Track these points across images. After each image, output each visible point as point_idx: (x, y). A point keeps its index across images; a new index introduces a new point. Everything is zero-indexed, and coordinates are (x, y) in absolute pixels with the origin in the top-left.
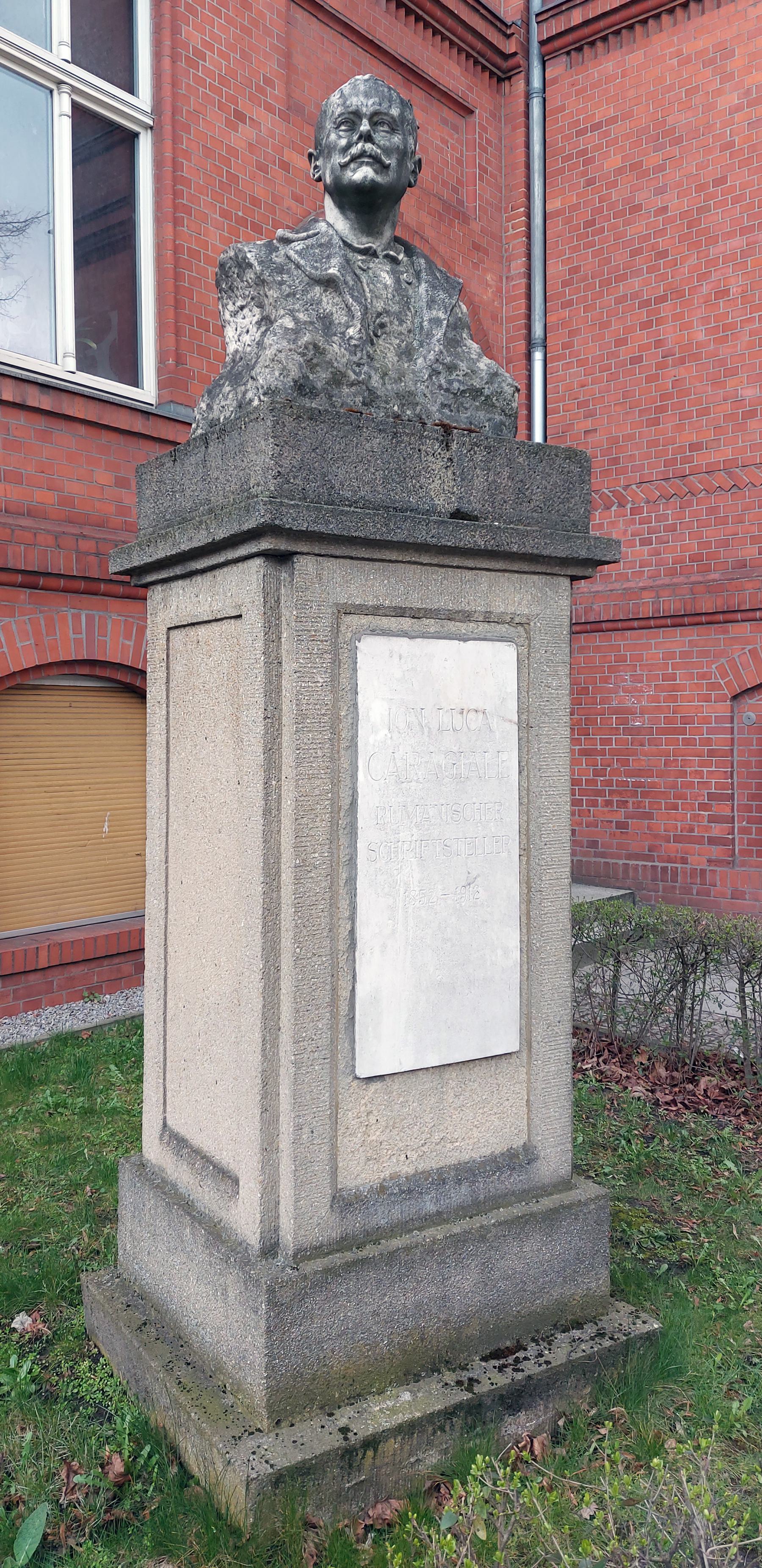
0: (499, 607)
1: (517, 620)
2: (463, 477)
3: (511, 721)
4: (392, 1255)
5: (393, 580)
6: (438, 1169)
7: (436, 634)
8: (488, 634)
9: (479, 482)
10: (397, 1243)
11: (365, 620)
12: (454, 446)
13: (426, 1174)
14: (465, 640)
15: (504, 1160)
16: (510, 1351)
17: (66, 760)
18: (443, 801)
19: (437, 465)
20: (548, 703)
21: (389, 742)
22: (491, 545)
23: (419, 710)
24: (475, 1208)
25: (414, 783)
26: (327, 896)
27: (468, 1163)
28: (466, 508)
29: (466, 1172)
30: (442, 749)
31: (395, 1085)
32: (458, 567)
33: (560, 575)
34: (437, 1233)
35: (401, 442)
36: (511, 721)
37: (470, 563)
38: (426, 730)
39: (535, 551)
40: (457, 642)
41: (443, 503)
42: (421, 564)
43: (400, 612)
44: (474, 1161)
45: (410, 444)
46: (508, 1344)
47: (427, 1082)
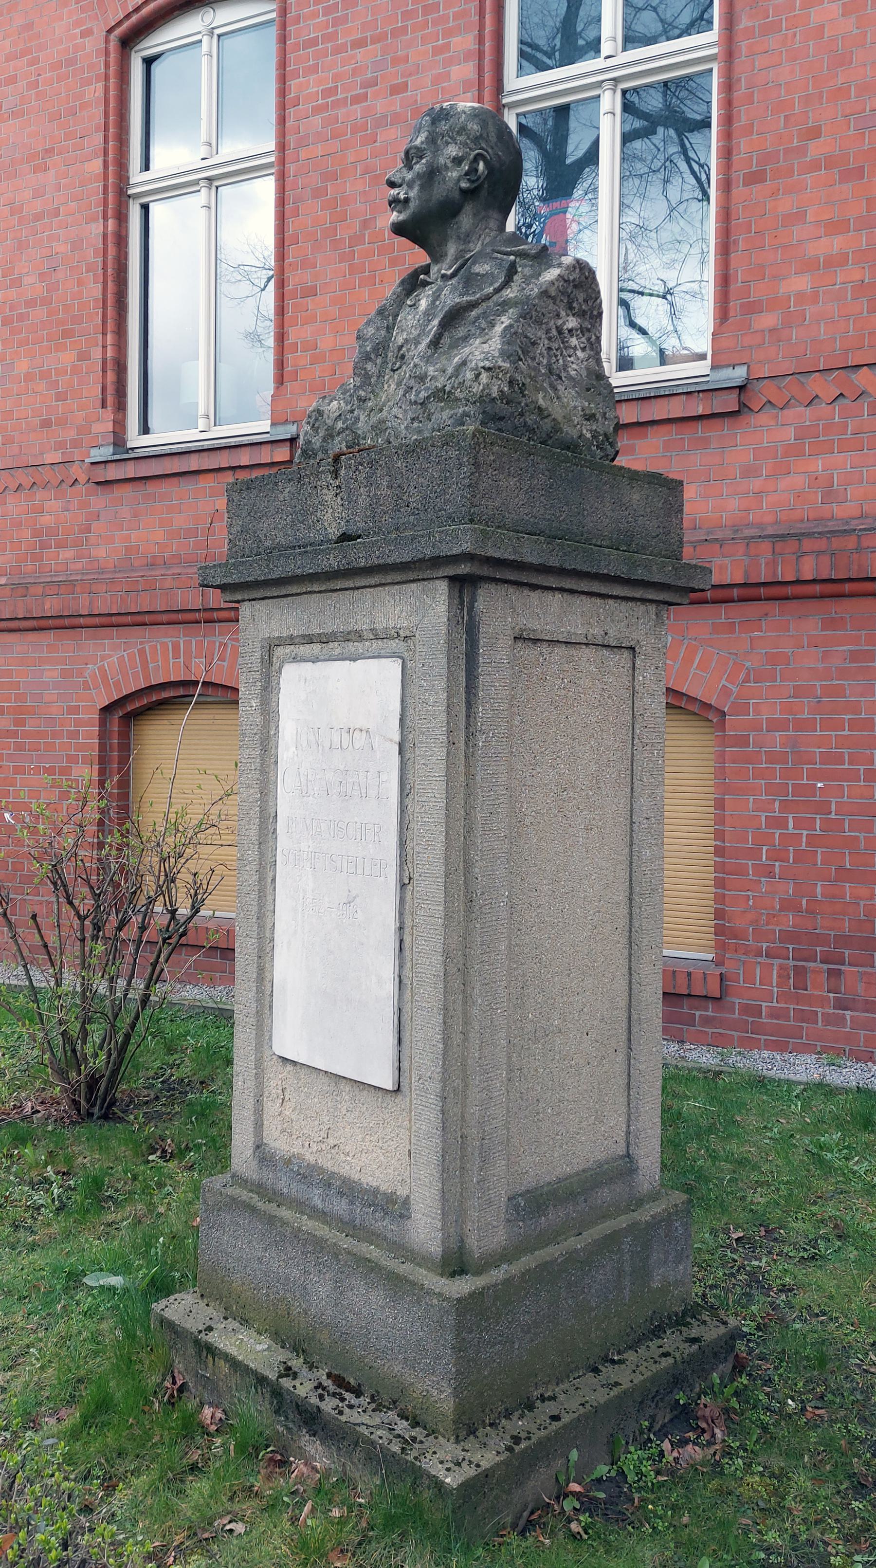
0: (381, 624)
1: (402, 633)
2: (350, 501)
3: (391, 740)
4: (271, 1220)
5: (299, 611)
6: (332, 1173)
7: (340, 656)
8: (382, 651)
9: (363, 501)
10: (285, 1213)
11: (288, 649)
12: (342, 472)
13: (321, 1170)
14: (355, 660)
15: (382, 1200)
16: (349, 1388)
17: (680, 763)
18: (331, 817)
19: (329, 495)
20: (425, 721)
21: (296, 758)
22: (344, 565)
23: (316, 730)
24: (350, 1228)
25: (311, 798)
26: (256, 888)
27: (354, 1182)
28: (352, 530)
29: (349, 1189)
30: (332, 767)
31: (303, 1072)
32: (341, 590)
33: (433, 578)
34: (308, 1224)
35: (304, 484)
36: (391, 740)
37: (350, 584)
38: (321, 748)
39: (381, 561)
40: (348, 662)
41: (334, 532)
42: (315, 592)
43: (309, 639)
44: (360, 1184)
45: (310, 483)
46: (352, 1381)
47: (323, 1083)
